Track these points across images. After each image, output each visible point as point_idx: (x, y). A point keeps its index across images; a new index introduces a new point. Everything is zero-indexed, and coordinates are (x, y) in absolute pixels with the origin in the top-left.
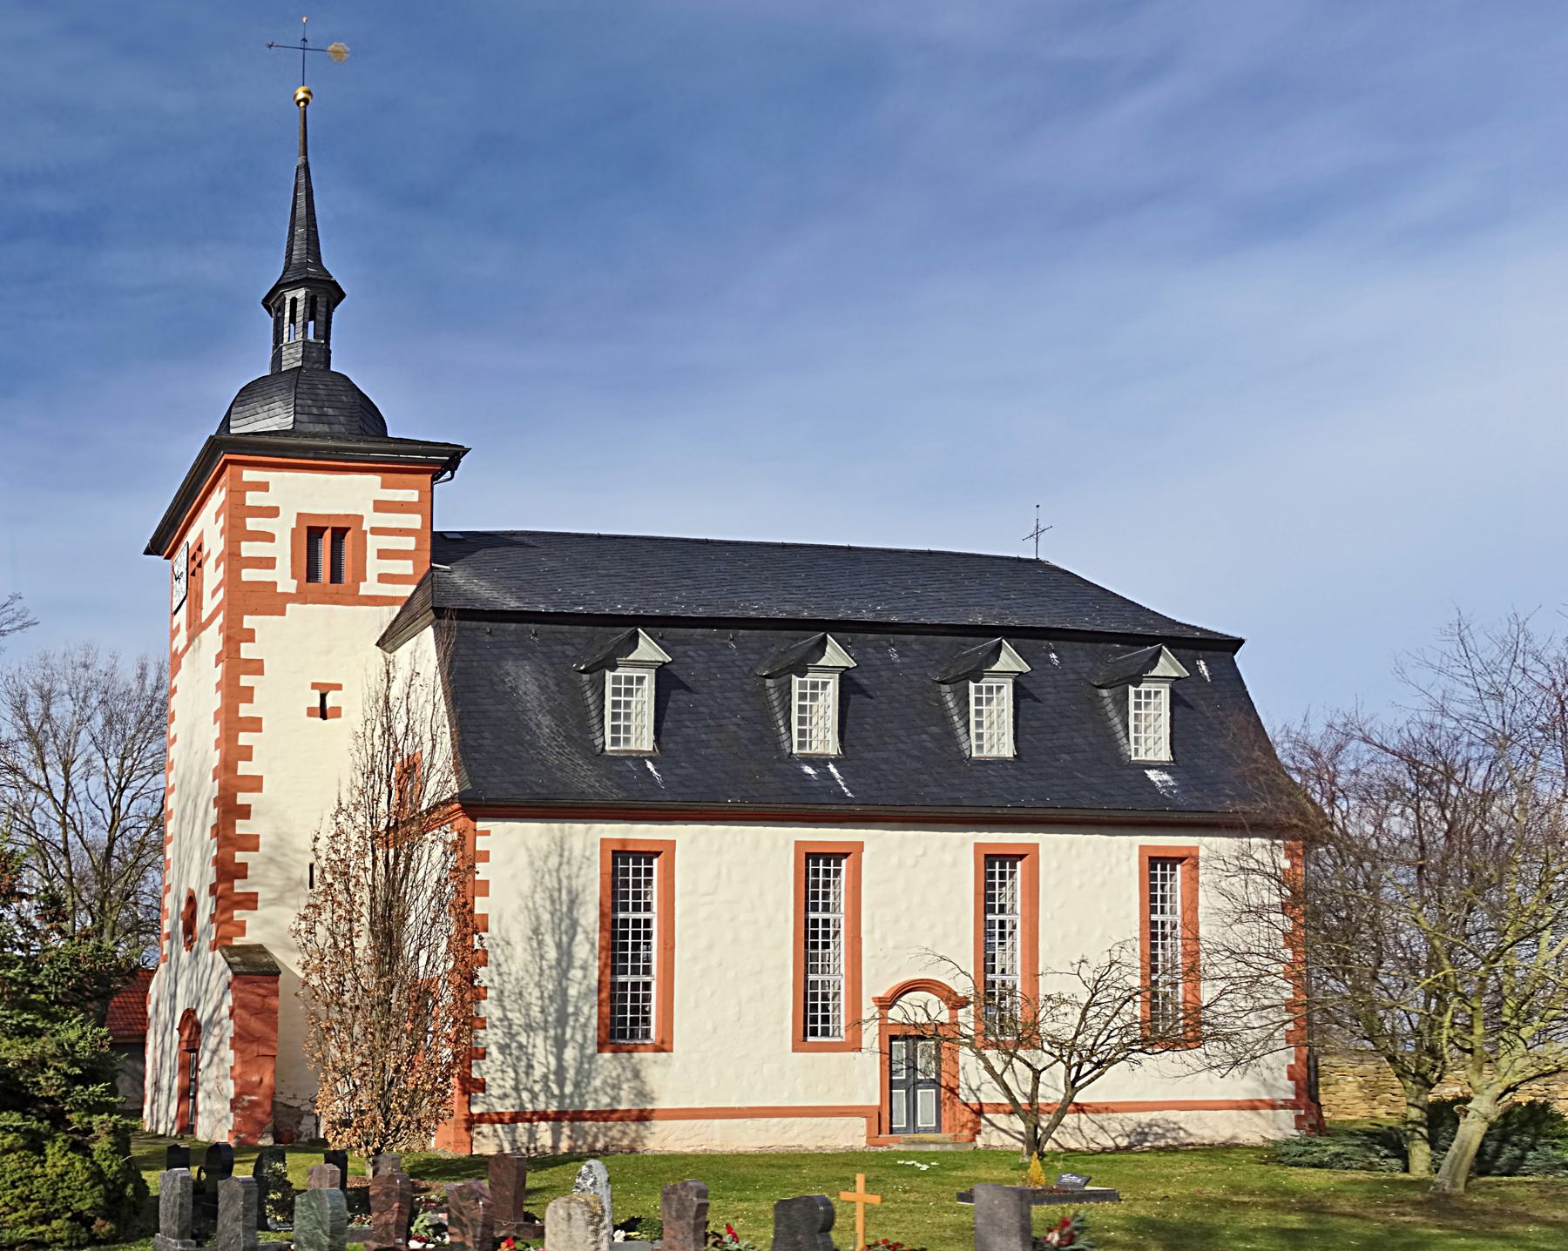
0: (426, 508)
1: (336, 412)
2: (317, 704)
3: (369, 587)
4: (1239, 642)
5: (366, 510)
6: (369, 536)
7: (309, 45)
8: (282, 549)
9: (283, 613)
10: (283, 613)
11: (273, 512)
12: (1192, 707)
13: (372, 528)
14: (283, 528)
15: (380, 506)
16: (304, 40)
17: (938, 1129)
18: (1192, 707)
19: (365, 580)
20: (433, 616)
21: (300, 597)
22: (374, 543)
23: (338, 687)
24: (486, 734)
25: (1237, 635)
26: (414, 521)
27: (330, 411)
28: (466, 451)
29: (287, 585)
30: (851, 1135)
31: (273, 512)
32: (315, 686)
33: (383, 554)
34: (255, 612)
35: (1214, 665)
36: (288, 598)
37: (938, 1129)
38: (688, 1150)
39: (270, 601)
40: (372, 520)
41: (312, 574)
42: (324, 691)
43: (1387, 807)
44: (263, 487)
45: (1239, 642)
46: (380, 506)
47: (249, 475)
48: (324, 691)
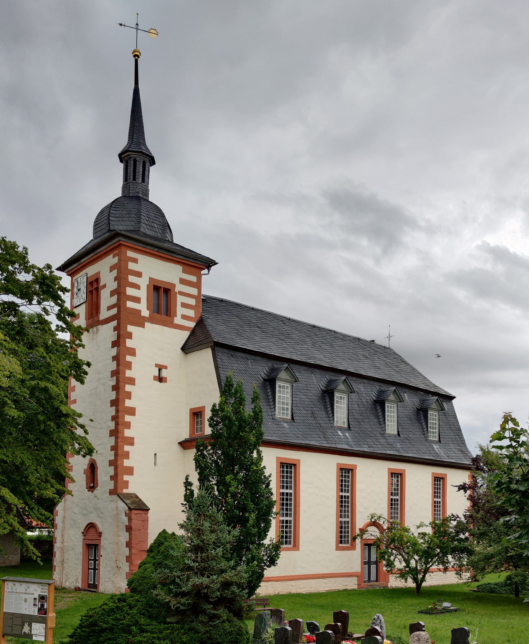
0: (198, 285)
3: (178, 320)
4: (454, 397)
5: (176, 282)
6: (178, 295)
7: (140, 27)
8: (142, 293)
9: (143, 326)
10: (143, 326)
11: (139, 274)
13: (179, 291)
14: (143, 282)
15: (183, 281)
16: (137, 24)
17: (377, 581)
19: (176, 316)
20: (213, 344)
21: (151, 320)
22: (180, 299)
23: (166, 367)
26: (194, 291)
28: (216, 264)
29: (145, 313)
30: (352, 584)
31: (139, 274)
32: (157, 365)
33: (184, 305)
35: (457, 427)
36: (145, 319)
37: (377, 581)
39: (140, 322)
40: (179, 287)
41: (158, 311)
42: (160, 368)
43: (208, 556)
44: (135, 261)
45: (454, 397)
47: (130, 254)
48: (160, 368)
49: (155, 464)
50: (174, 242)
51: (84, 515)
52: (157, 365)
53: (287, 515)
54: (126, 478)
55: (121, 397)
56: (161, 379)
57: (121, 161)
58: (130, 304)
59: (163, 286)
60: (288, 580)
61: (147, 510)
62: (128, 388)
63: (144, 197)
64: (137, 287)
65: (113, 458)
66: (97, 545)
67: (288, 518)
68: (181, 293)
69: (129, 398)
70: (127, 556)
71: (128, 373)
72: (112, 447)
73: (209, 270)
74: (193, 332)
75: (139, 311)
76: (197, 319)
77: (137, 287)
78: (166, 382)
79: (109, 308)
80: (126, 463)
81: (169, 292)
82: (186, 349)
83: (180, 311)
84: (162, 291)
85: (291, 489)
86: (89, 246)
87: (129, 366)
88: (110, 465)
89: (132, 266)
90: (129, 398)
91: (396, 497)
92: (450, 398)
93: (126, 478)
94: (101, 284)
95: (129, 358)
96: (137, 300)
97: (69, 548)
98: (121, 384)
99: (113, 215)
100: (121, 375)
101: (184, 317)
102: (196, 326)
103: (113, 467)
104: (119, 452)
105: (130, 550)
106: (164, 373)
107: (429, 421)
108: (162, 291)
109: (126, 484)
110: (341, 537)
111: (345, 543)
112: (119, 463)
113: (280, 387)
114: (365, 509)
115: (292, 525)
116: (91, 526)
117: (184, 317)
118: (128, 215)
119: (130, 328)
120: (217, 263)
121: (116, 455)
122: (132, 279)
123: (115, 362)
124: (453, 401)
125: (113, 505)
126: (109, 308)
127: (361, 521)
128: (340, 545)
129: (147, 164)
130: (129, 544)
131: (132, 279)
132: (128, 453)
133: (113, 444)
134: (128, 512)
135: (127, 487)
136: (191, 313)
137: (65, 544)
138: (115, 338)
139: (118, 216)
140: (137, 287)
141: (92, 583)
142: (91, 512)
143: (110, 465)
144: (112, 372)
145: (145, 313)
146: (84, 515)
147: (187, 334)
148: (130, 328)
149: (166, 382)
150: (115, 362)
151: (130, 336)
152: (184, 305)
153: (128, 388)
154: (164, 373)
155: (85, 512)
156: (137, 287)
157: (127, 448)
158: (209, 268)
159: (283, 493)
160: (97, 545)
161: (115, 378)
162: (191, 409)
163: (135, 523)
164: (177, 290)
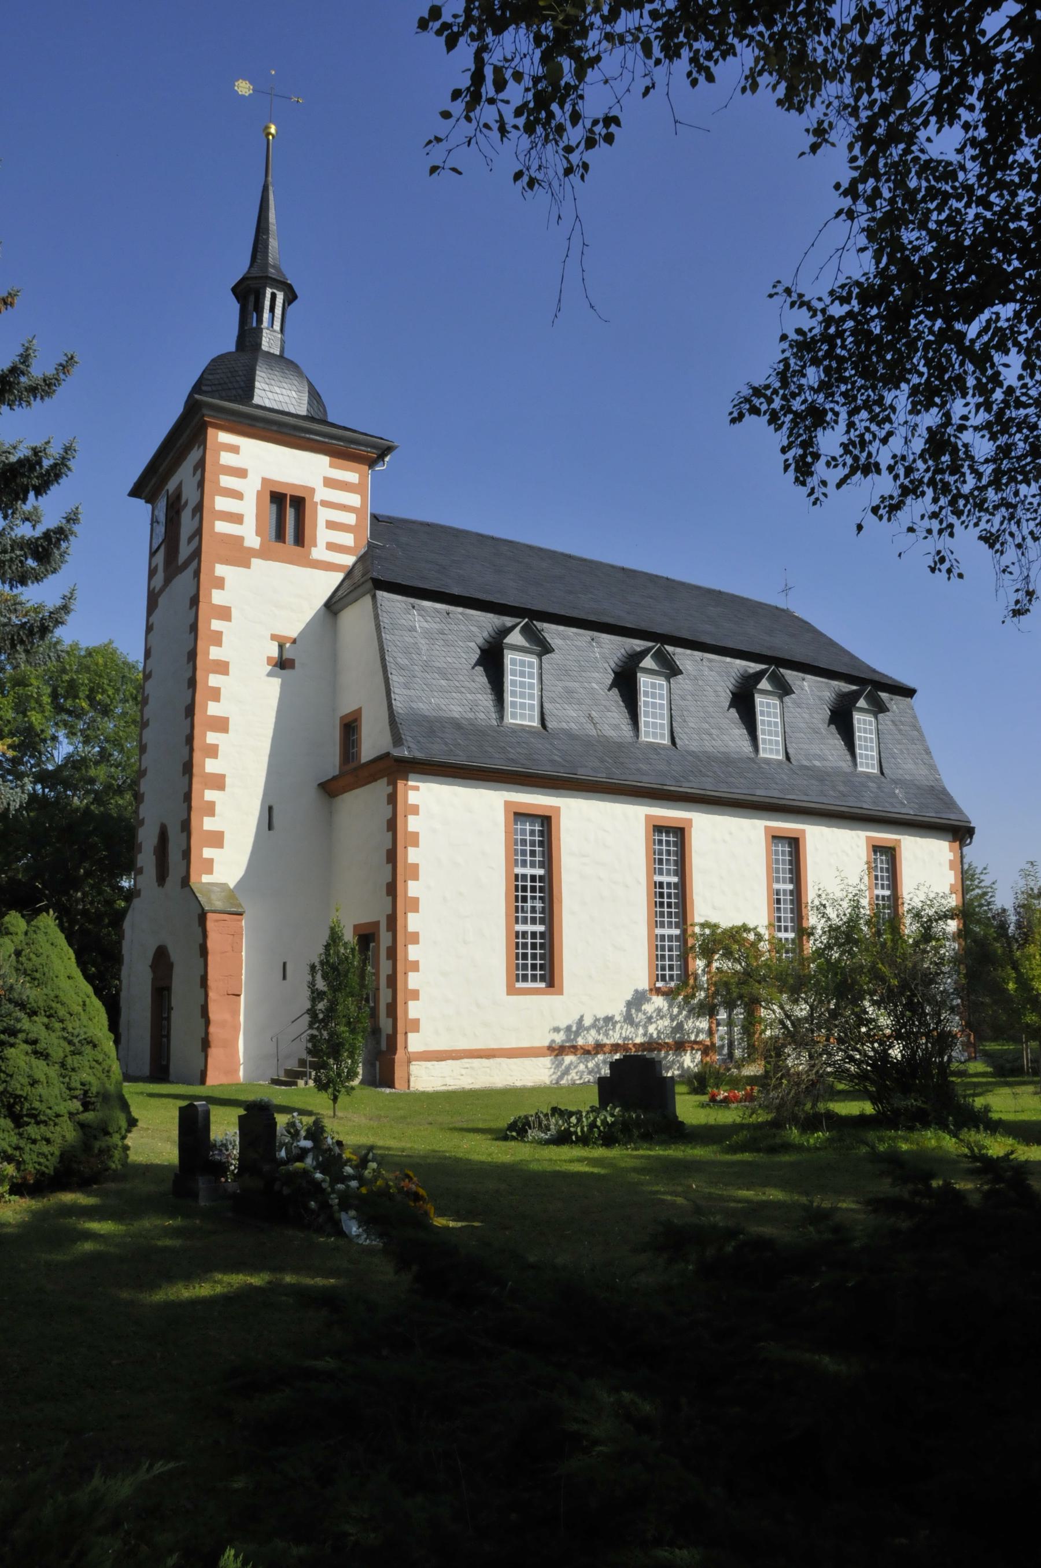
3: (319, 552)
5: (317, 483)
6: (319, 507)
8: (248, 507)
11: (241, 473)
14: (251, 487)
15: (329, 483)
19: (315, 546)
21: (264, 553)
22: (324, 515)
29: (253, 541)
31: (241, 473)
33: (331, 525)
39: (240, 556)
40: (322, 493)
44: (235, 449)
46: (329, 483)
58: (222, 527)
59: (289, 492)
68: (326, 504)
74: (349, 574)
83: (323, 535)
89: (227, 459)
94: (183, 501)
96: (237, 518)
101: (331, 547)
113: (513, 662)
117: (331, 547)
131: (227, 481)
135: (210, 872)
136: (347, 539)
140: (238, 495)
147: (339, 577)
148: (220, 570)
151: (220, 583)
152: (331, 525)
164: (317, 498)
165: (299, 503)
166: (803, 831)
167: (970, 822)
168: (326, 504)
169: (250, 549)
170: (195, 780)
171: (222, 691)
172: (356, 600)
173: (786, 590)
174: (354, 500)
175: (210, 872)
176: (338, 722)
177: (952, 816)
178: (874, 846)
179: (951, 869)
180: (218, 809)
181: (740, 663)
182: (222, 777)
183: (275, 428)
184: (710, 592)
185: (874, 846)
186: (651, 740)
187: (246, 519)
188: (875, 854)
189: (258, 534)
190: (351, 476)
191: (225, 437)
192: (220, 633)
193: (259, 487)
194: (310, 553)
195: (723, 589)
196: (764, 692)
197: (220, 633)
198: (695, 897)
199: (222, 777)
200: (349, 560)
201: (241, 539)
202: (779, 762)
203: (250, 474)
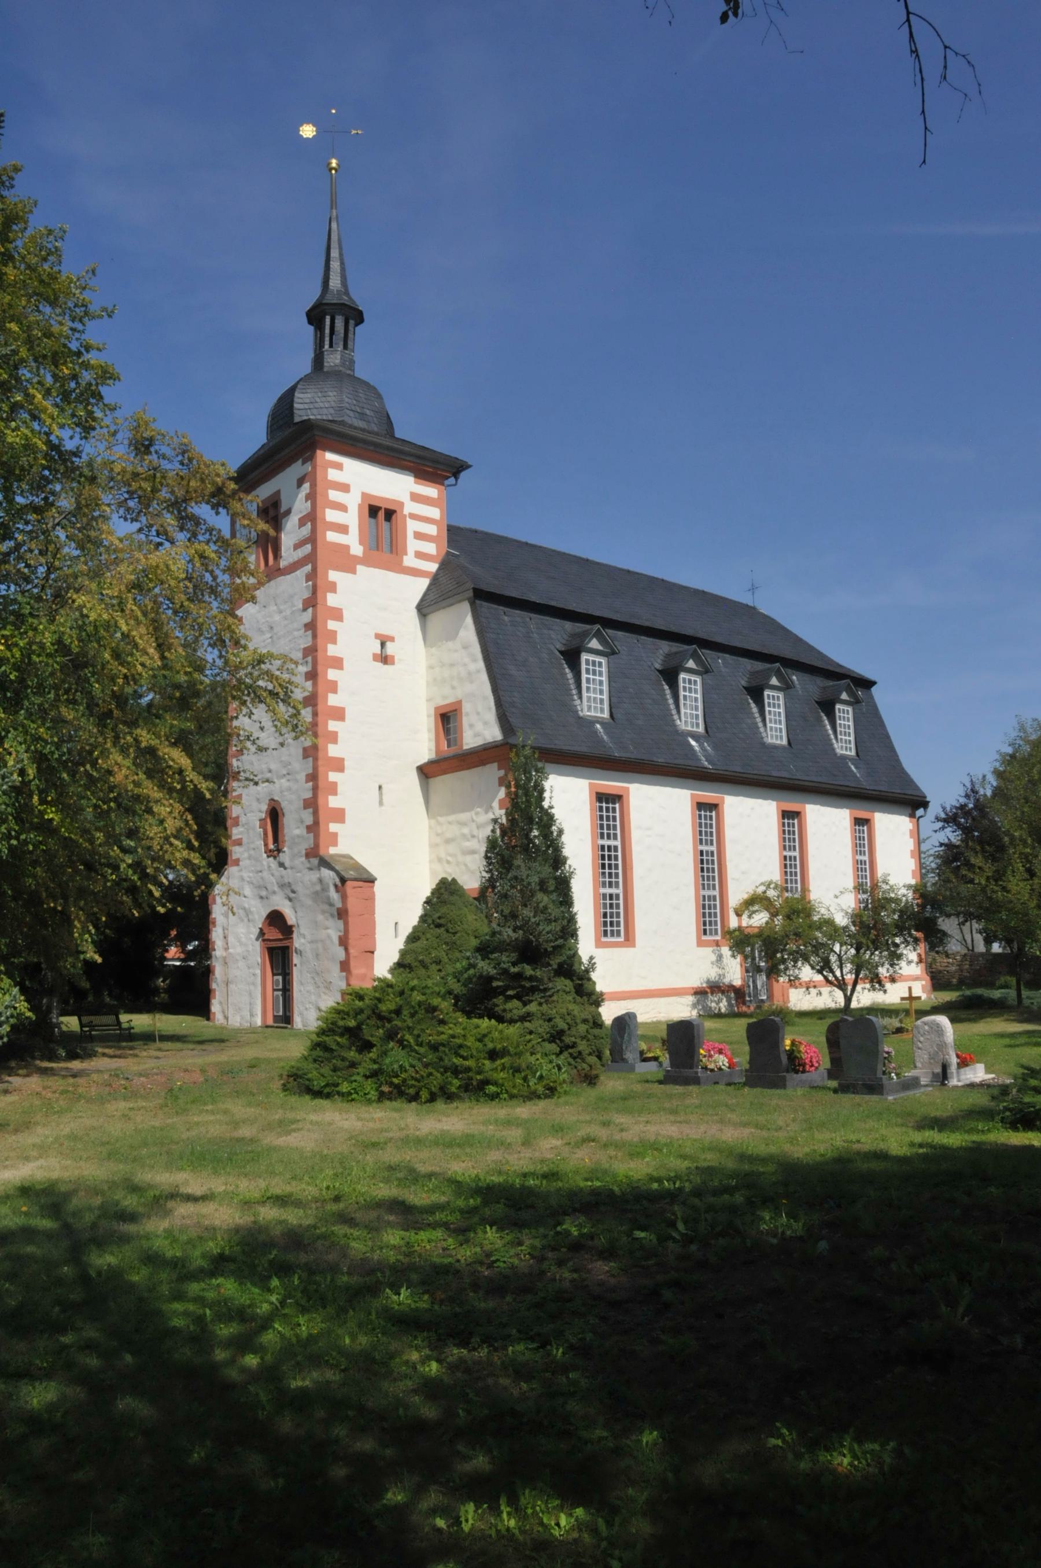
1: (372, 414)
2: (378, 650)
3: (410, 560)
4: (873, 683)
5: (405, 498)
6: (408, 519)
8: (352, 518)
11: (345, 488)
12: (222, 1041)
14: (353, 501)
15: (415, 497)
18: (222, 1041)
21: (366, 561)
22: (412, 526)
24: (516, 694)
25: (470, 463)
27: (368, 412)
28: (468, 467)
29: (357, 550)
31: (345, 488)
32: (378, 636)
33: (418, 536)
34: (337, 568)
35: (614, 684)
38: (649, 1021)
39: (349, 564)
40: (410, 507)
44: (339, 466)
45: (873, 683)
46: (415, 497)
49: (381, 803)
50: (397, 435)
51: (261, 898)
52: (378, 636)
53: (610, 885)
54: (333, 827)
55: (321, 690)
56: (385, 659)
57: (310, 322)
58: (332, 536)
59: (384, 505)
60: (624, 999)
61: (371, 881)
62: (332, 674)
63: (349, 372)
64: (342, 508)
65: (309, 795)
66: (287, 948)
67: (613, 891)
68: (414, 517)
69: (335, 691)
70: (341, 962)
71: (332, 650)
72: (307, 776)
73: (456, 479)
74: (435, 580)
75: (347, 548)
76: (440, 558)
77: (343, 508)
78: (393, 663)
79: (297, 547)
80: (333, 802)
81: (394, 517)
82: (424, 609)
83: (413, 545)
84: (381, 515)
85: (615, 838)
86: (262, 452)
87: (332, 637)
88: (305, 808)
89: (333, 474)
90: (335, 691)
91: (792, 854)
92: (867, 684)
93: (333, 827)
94: (283, 509)
95: (332, 625)
96: (343, 529)
97: (238, 957)
98: (320, 669)
99: (300, 401)
100: (320, 654)
101: (419, 555)
102: (439, 569)
103: (311, 810)
104: (321, 784)
105: (346, 950)
106: (390, 649)
107: (838, 722)
108: (381, 515)
109: (334, 839)
110: (705, 924)
111: (711, 934)
112: (321, 801)
113: (587, 662)
114: (743, 873)
115: (621, 902)
116: (276, 919)
117: (419, 555)
118: (324, 399)
119: (333, 575)
120: (470, 466)
121: (315, 789)
122: (334, 495)
123: (309, 633)
124: (874, 689)
125: (314, 876)
126: (297, 547)
127: (736, 895)
128: (704, 938)
129: (352, 322)
130: (344, 942)
131: (334, 495)
132: (334, 785)
133: (310, 771)
134: (339, 883)
135: (335, 844)
136: (431, 548)
137: (231, 950)
138: (307, 595)
139: (308, 401)
140: (343, 508)
141: (281, 1013)
142: (274, 892)
143: (305, 808)
144: (305, 649)
145: (357, 550)
146: (261, 898)
147: (424, 583)
148: (333, 575)
149: (393, 663)
150: (309, 633)
151: (333, 587)
152: (418, 536)
153: (332, 674)
154: (390, 649)
155: (264, 893)
156: (342, 508)
157: (333, 776)
158: (456, 475)
159: (603, 847)
160: (287, 948)
161: (309, 659)
162: (436, 709)
163: (353, 904)
164: (406, 511)
165: (390, 514)
166: (628, 788)
167: (925, 797)
168: (414, 517)
169: (355, 557)
170: (320, 763)
171: (339, 684)
172: (452, 605)
173: (753, 589)
174: (435, 513)
175: (335, 844)
176: (432, 712)
177: (909, 792)
178: (597, 794)
179: (911, 837)
180: (340, 789)
181: (568, 626)
182: (342, 760)
183: (371, 448)
184: (697, 592)
185: (597, 794)
186: (844, 752)
187: (350, 529)
188: (700, 810)
189: (361, 543)
190: (431, 491)
191: (330, 456)
192: (335, 632)
193: (359, 500)
194: (402, 561)
195: (665, 578)
196: (690, 671)
197: (335, 632)
198: (728, 864)
199: (342, 760)
200: (433, 567)
201: (348, 547)
202: (782, 747)
203: (352, 489)
